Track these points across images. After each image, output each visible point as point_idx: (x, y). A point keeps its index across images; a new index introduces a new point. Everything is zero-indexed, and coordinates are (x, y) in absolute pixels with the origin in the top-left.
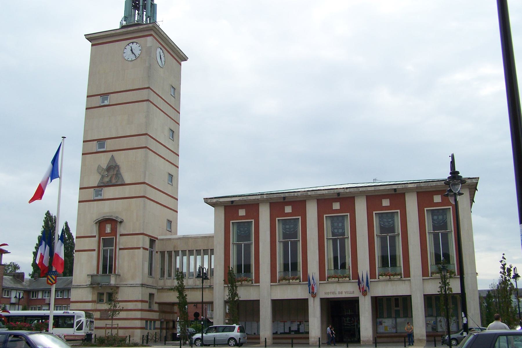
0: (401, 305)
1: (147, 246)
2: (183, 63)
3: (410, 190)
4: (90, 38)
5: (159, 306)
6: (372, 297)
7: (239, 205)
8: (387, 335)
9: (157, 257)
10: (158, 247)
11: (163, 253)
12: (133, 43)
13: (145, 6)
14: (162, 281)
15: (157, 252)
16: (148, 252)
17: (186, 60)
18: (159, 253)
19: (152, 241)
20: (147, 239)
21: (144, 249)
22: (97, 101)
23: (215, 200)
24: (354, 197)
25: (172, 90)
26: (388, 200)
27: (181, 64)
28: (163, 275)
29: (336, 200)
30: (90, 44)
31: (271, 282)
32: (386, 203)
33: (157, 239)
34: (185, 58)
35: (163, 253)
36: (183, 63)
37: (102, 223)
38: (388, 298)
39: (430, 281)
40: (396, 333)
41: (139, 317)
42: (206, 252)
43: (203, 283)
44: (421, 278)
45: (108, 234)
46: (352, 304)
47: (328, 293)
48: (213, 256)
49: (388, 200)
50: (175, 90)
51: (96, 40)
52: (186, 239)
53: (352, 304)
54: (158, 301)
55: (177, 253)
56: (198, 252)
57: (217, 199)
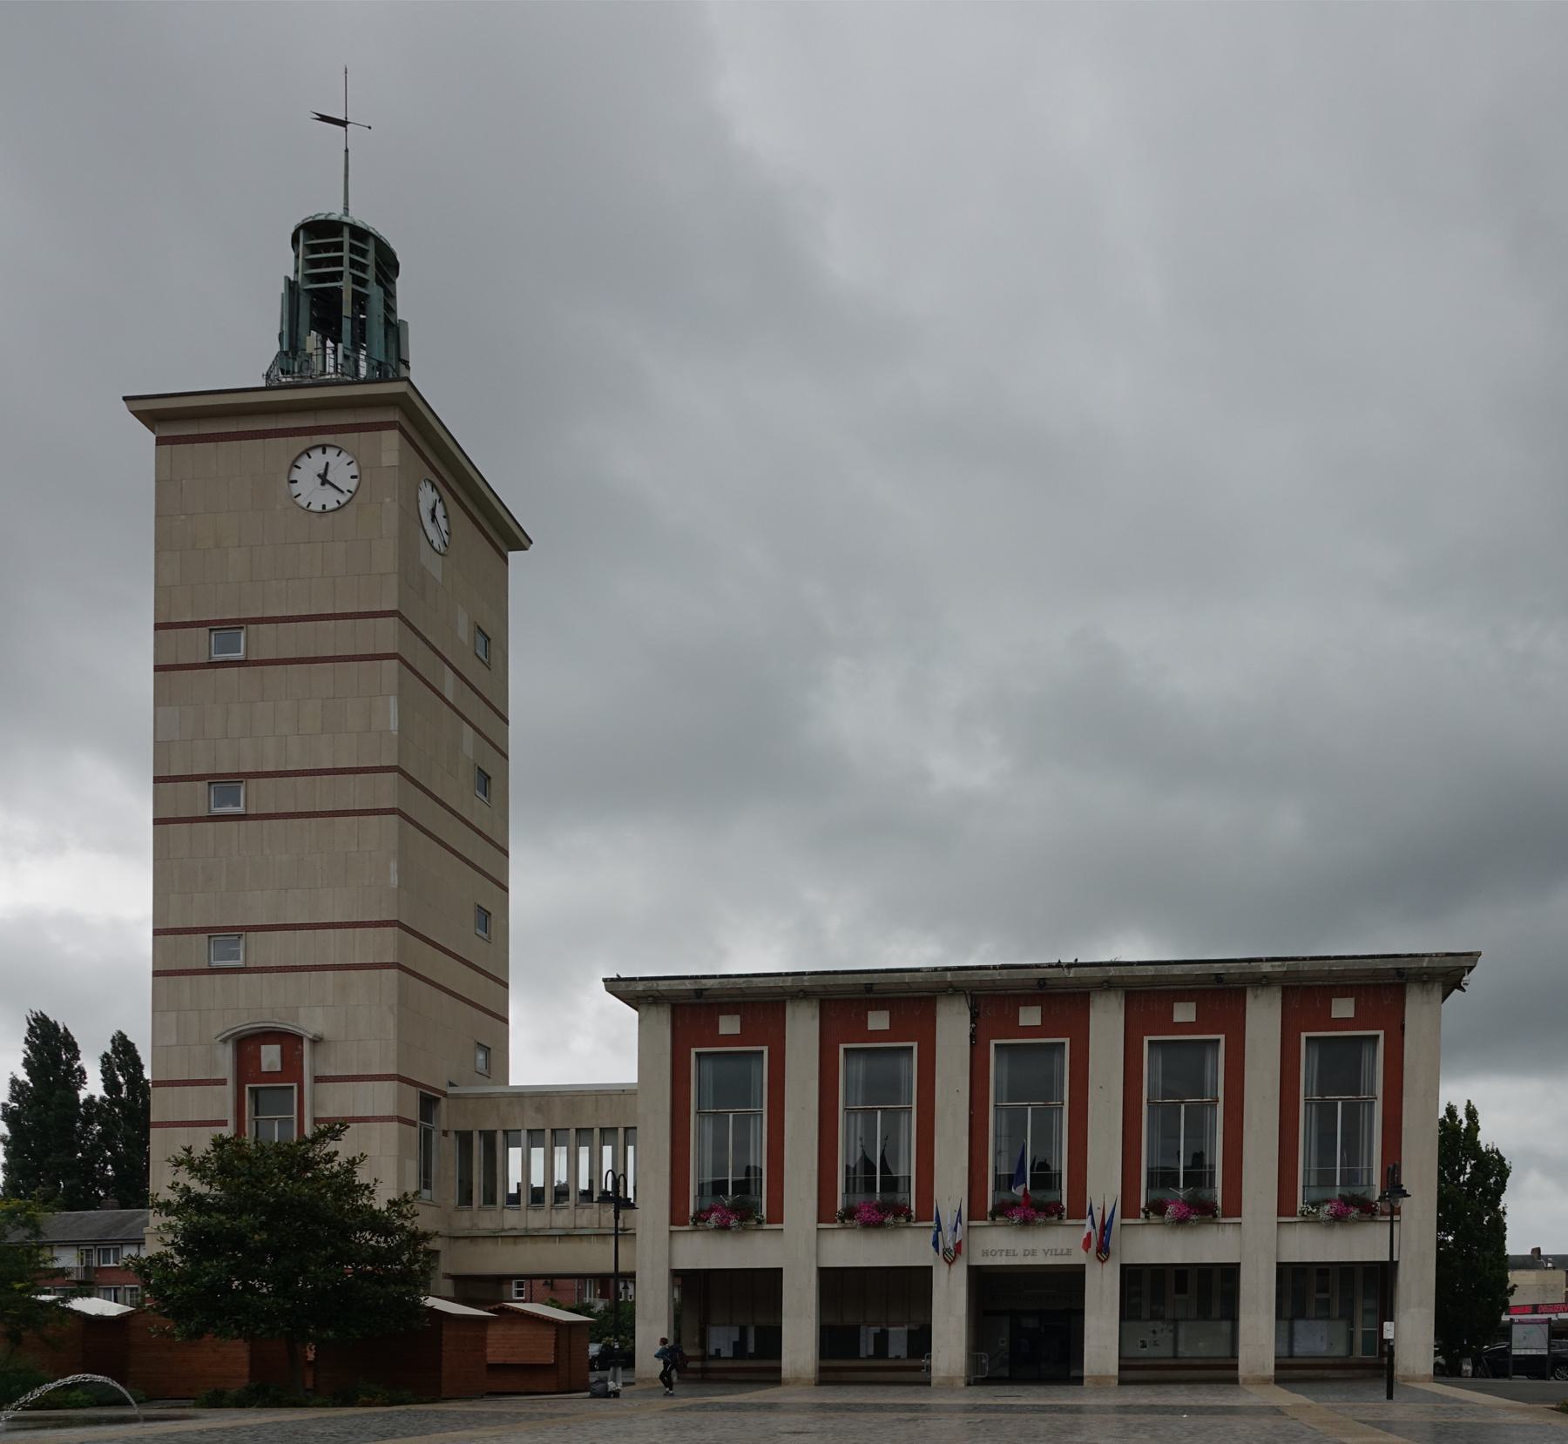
0: (1215, 1288)
1: (413, 1113)
2: (511, 555)
3: (1263, 981)
4: (159, 414)
5: (456, 1286)
6: (1123, 1267)
7: (720, 1004)
8: (1330, 1362)
9: (446, 1152)
10: (445, 1116)
11: (465, 1139)
12: (324, 448)
13: (363, 332)
14: (466, 1215)
15: (445, 1133)
16: (415, 1131)
17: (525, 549)
18: (452, 1135)
19: (429, 1102)
20: (413, 1094)
21: (401, 1120)
22: (198, 645)
23: (640, 987)
24: (1088, 994)
25: (481, 640)
26: (1193, 1005)
27: (506, 559)
28: (466, 1198)
29: (1030, 1000)
30: (153, 437)
31: (819, 1221)
32: (1184, 1013)
33: (445, 1095)
34: (513, 538)
35: (465, 1139)
36: (511, 555)
37: (246, 1044)
38: (1158, 1271)
39: (1298, 1226)
40: (1175, 1357)
41: (488, 1247)
42: (607, 1134)
43: (617, 1218)
44: (1274, 1218)
45: (271, 1076)
46: (1066, 1284)
47: (994, 1253)
48: (631, 1149)
49: (1193, 1005)
50: (490, 644)
51: (173, 419)
52: (542, 1098)
53: (1066, 1284)
54: (453, 1272)
55: (511, 1138)
56: (583, 1134)
57: (649, 984)
